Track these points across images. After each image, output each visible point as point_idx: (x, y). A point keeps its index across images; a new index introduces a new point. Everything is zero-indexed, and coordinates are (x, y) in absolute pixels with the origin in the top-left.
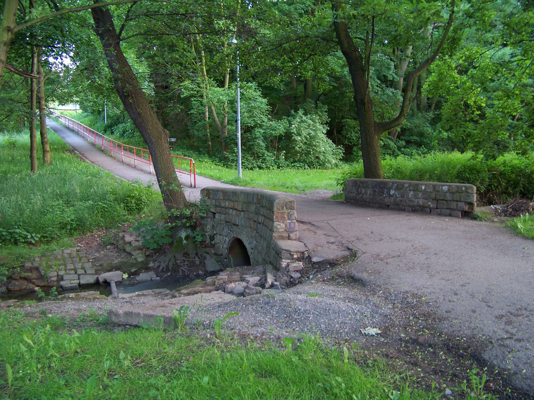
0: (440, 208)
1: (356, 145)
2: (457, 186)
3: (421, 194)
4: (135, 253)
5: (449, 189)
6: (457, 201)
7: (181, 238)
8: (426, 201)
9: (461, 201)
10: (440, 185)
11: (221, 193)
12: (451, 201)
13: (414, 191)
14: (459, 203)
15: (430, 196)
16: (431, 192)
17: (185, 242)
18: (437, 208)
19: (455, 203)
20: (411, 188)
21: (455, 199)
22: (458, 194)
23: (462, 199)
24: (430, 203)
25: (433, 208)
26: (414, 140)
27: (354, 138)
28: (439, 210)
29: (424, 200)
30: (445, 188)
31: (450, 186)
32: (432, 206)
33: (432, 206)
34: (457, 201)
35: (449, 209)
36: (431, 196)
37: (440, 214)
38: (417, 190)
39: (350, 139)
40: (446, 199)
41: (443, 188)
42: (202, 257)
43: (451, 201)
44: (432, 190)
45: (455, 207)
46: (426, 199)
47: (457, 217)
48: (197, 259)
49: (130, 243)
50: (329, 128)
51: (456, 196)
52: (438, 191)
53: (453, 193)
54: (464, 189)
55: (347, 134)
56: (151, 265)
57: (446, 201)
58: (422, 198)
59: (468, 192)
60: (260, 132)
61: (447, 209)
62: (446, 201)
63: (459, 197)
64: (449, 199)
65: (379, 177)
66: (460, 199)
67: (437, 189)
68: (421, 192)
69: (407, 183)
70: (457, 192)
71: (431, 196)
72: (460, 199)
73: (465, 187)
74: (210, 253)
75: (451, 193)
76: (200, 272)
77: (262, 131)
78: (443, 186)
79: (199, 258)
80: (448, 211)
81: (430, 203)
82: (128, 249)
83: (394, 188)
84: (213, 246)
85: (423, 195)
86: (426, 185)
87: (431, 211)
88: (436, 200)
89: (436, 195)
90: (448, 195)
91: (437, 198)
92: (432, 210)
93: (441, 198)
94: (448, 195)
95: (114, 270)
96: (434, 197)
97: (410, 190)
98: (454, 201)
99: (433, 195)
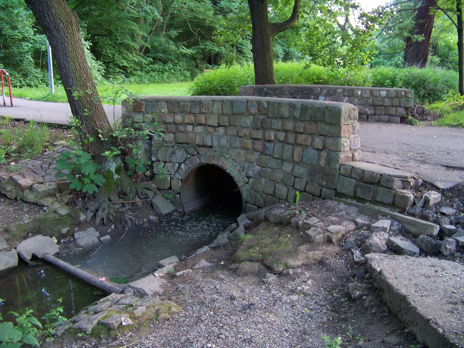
0: (378, 115)
1: (112, 62)
2: (395, 91)
3: (356, 100)
4: (48, 201)
5: (387, 94)
6: (396, 106)
7: (109, 171)
8: (363, 107)
9: (400, 107)
10: (377, 90)
11: (165, 105)
12: (389, 106)
13: (348, 96)
14: (398, 109)
15: (367, 102)
16: (368, 98)
17: (116, 176)
18: (375, 115)
19: (394, 109)
20: (346, 94)
21: (394, 105)
22: (397, 99)
23: (402, 105)
24: (367, 109)
25: (371, 115)
26: (160, 57)
27: (110, 55)
28: (377, 117)
29: (360, 107)
30: (383, 93)
31: (388, 91)
32: (369, 112)
33: (369, 112)
34: (396, 106)
35: (387, 115)
36: (369, 101)
37: (378, 121)
38: (353, 96)
39: (105, 56)
40: (385, 105)
41: (381, 93)
42: (142, 195)
43: (389, 106)
44: (368, 96)
45: (395, 113)
46: (363, 105)
47: (397, 123)
48: (138, 200)
49: (31, 188)
50: (92, 44)
51: (396, 102)
52: (376, 97)
53: (392, 98)
54: (403, 93)
55: (103, 51)
56: (83, 217)
57: (384, 107)
58: (358, 105)
59: (408, 97)
60: (28, 46)
61: (385, 115)
62: (384, 107)
63: (398, 103)
64: (387, 104)
65: (274, 83)
66: (400, 104)
67: (375, 94)
68: (357, 97)
69: (340, 88)
70: (397, 97)
71: (369, 101)
72: (400, 104)
73: (405, 91)
74: (152, 189)
75: (389, 98)
76: (151, 217)
77: (30, 45)
78: (380, 91)
79: (139, 198)
80: (387, 118)
81: (367, 109)
82: (31, 197)
83: (324, 93)
84: (153, 177)
85: (359, 100)
86: (362, 90)
87: (367, 117)
88: (374, 106)
89: (373, 100)
90: (386, 100)
91: (375, 103)
92: (370, 117)
93: (379, 104)
94: (386, 100)
95: (30, 235)
96: (371, 102)
97: (344, 96)
98: (393, 106)
99: (370, 101)
